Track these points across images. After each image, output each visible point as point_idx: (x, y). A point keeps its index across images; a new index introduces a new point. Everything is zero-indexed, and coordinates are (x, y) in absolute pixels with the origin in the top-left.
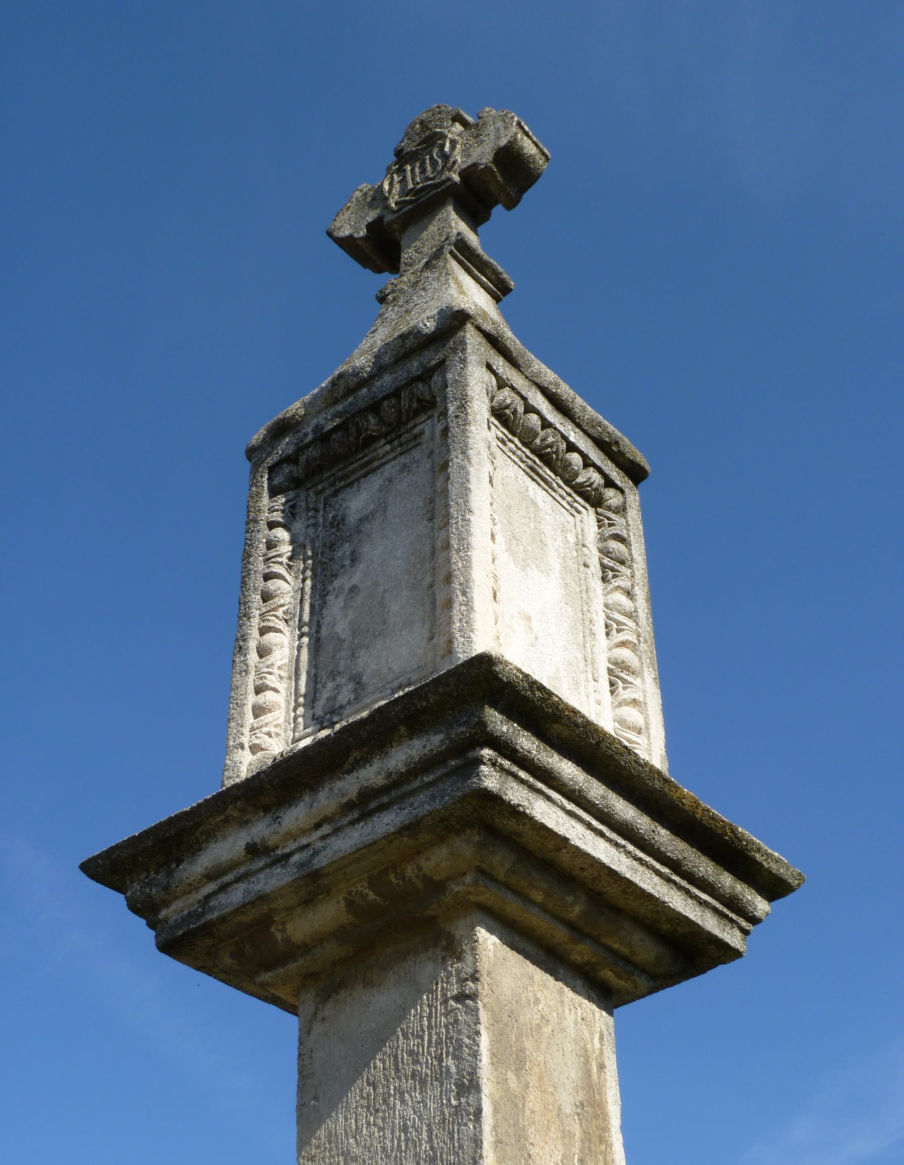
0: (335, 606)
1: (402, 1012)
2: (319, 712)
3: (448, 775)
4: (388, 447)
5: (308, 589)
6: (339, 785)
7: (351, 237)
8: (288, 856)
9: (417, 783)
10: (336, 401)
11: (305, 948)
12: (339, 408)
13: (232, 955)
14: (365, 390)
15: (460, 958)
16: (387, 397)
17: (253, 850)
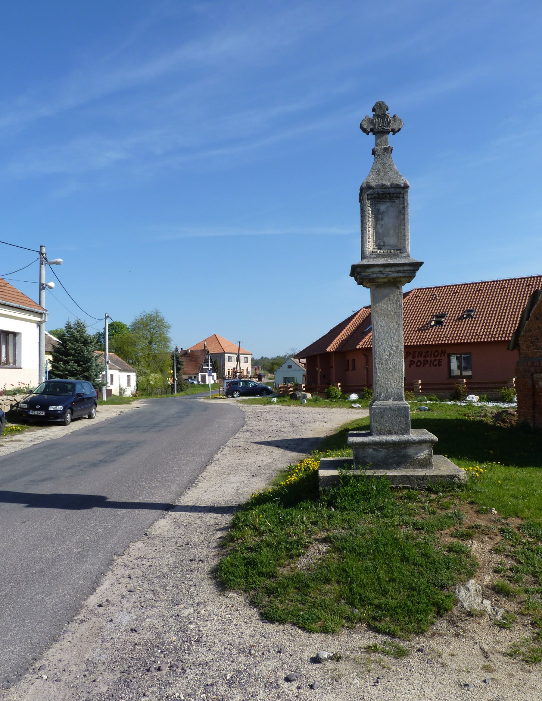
0: (379, 227)
6: (395, 268)
7: (366, 129)
11: (379, 282)
12: (383, 190)
15: (400, 289)
17: (380, 271)
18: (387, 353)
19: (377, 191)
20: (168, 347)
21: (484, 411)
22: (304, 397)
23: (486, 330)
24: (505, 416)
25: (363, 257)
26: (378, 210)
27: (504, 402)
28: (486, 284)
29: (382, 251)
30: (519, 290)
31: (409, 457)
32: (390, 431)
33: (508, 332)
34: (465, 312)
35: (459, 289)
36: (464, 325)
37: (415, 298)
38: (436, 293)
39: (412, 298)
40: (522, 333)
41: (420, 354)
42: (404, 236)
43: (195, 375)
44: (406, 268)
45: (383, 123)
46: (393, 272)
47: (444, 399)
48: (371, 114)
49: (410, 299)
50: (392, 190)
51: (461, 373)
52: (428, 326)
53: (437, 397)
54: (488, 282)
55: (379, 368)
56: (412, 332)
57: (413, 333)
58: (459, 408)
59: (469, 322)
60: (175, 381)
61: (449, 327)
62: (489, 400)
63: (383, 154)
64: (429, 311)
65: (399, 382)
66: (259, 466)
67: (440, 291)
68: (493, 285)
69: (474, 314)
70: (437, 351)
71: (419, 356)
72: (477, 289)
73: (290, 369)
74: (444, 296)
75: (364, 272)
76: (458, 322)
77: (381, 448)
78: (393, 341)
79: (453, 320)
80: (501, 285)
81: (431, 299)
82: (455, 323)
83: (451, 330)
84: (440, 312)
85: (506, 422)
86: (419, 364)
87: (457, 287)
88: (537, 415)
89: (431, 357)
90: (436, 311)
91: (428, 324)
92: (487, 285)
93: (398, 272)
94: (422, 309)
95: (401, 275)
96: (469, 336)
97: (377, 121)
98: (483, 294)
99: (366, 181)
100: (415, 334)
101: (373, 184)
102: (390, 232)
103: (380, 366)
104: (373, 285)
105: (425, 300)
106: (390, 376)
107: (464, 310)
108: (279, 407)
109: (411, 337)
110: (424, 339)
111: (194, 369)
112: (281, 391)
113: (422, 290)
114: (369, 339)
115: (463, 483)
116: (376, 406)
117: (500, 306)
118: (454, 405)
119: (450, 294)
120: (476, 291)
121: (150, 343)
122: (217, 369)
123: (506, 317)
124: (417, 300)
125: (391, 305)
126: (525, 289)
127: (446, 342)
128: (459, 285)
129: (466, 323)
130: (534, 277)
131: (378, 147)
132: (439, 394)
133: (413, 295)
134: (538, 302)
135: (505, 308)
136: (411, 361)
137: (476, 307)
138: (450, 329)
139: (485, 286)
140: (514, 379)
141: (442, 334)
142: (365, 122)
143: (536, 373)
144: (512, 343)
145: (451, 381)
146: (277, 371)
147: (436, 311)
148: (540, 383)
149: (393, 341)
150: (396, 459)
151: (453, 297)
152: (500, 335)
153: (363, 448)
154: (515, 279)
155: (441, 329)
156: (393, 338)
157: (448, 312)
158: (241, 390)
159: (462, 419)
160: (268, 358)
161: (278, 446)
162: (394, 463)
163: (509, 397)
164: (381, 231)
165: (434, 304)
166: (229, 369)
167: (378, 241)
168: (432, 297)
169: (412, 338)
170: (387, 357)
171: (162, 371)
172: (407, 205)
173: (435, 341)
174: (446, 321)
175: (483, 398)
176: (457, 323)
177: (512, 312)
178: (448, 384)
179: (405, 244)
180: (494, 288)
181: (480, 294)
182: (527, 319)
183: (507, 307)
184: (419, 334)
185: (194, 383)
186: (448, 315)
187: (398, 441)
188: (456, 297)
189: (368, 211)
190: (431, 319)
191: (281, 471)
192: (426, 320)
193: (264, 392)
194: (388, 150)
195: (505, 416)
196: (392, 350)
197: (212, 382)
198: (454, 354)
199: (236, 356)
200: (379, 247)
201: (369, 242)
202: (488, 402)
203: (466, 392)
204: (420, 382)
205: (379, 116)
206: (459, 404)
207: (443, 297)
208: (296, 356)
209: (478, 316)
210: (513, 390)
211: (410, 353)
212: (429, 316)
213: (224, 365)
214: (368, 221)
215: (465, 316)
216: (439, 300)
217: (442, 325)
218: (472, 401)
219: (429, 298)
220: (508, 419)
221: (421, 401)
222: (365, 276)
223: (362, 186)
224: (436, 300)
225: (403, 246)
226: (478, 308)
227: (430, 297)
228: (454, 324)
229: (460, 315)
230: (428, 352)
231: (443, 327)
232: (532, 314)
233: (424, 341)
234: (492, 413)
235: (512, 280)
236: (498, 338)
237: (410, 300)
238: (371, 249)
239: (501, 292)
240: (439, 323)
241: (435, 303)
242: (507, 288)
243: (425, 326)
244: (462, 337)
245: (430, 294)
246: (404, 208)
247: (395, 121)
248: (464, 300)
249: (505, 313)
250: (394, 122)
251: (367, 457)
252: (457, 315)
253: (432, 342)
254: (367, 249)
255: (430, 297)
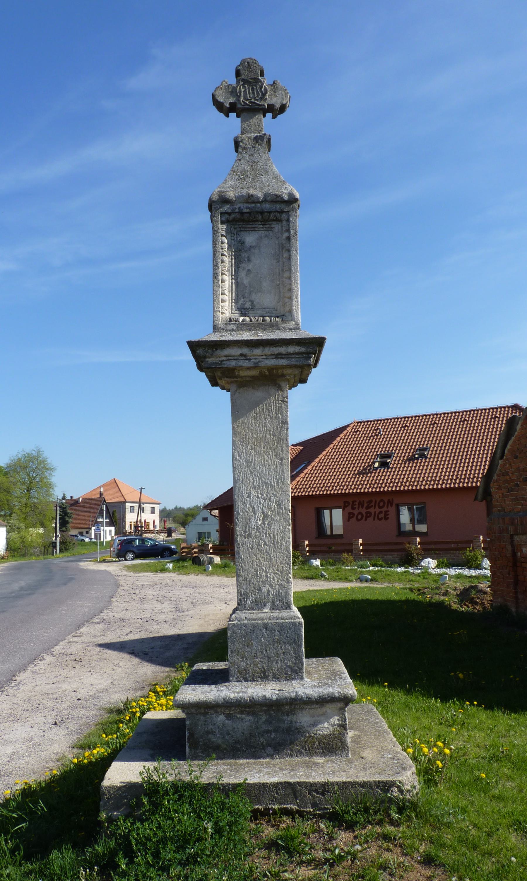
0: (242, 274)
1: (265, 399)
2: (239, 307)
3: (302, 357)
4: (262, 226)
5: (233, 263)
6: (272, 349)
7: (223, 103)
8: (251, 359)
9: (294, 356)
10: (248, 203)
11: (241, 377)
12: (249, 206)
13: (221, 373)
14: (259, 205)
15: (283, 391)
16: (267, 212)
17: (241, 355)
18: (259, 514)
19: (239, 208)
20: (51, 495)
21: (445, 586)
22: (211, 561)
23: (443, 474)
24: (475, 594)
25: (215, 329)
26: (241, 242)
27: (470, 568)
28: (442, 416)
29: (248, 319)
30: (482, 423)
31: (300, 731)
32: (264, 673)
33: (472, 476)
34: (417, 450)
35: (409, 422)
36: (415, 467)
37: (355, 434)
38: (380, 427)
39: (350, 433)
40: (495, 477)
41: (361, 504)
42: (290, 290)
43: (87, 530)
44: (292, 349)
45: (253, 93)
46: (267, 357)
47: (392, 564)
48: (232, 80)
49: (348, 434)
50: (267, 207)
51: (414, 527)
52: (370, 469)
53: (383, 560)
54: (444, 414)
55: (243, 543)
56: (351, 476)
57: (352, 477)
58: (412, 578)
59: (422, 464)
60: (58, 539)
61: (397, 469)
62: (450, 565)
63: (253, 147)
64: (371, 449)
65: (282, 573)
66: (79, 699)
67: (384, 424)
68: (451, 417)
69: (428, 454)
70: (382, 500)
71: (360, 507)
72: (431, 422)
73: (205, 522)
74: (390, 431)
75: (212, 356)
76: (409, 464)
77: (242, 712)
78: (271, 492)
79: (402, 460)
80: (460, 417)
81: (373, 434)
82: (405, 464)
83: (400, 473)
84: (389, 450)
85: (477, 603)
86: (360, 517)
87: (407, 419)
88: (520, 596)
89: (375, 508)
90: (380, 450)
91: (370, 466)
92: (443, 418)
93: (277, 356)
94: (363, 447)
95: (282, 362)
96: (422, 482)
97: (243, 90)
98: (438, 428)
99: (219, 189)
100: (355, 478)
101: (231, 195)
102: (265, 284)
103: (246, 540)
104: (232, 382)
105: (367, 435)
106: (265, 560)
107: (415, 448)
108: (174, 576)
109: (349, 482)
110: (366, 485)
111: (86, 523)
112: (183, 552)
113: (363, 424)
114: (296, 485)
115: (409, 801)
116: (235, 622)
117: (460, 443)
118: (405, 572)
119: (398, 428)
120: (430, 425)
121: (29, 490)
122: (116, 522)
123: (468, 457)
124: (356, 436)
125: (267, 422)
126: (490, 422)
127: (386, 489)
128: (408, 418)
129: (418, 464)
130: (501, 408)
131: (244, 136)
132: (385, 557)
133: (352, 430)
134: (516, 433)
135: (467, 446)
136: (350, 514)
137: (431, 444)
138: (398, 472)
139: (441, 419)
140: (481, 538)
141: (373, 480)
142: (221, 92)
143: (517, 534)
144: (481, 490)
145: (399, 540)
146: (190, 525)
147: (380, 450)
148: (524, 550)
149: (271, 492)
150: (273, 735)
151: (401, 432)
152: (462, 480)
153: (205, 714)
154: (478, 410)
155: (387, 472)
156: (271, 485)
157: (395, 450)
158: (136, 551)
159: (414, 600)
160: (183, 508)
161: (132, 653)
162: (269, 745)
163: (475, 561)
164: (246, 282)
165: (377, 440)
166: (131, 522)
167: (241, 301)
168: (375, 432)
169: (351, 483)
170: (260, 522)
171: (43, 525)
172: (296, 233)
173: (380, 488)
174: (393, 462)
175: (443, 563)
176: (407, 465)
177: (475, 451)
178: (397, 544)
179: (291, 305)
180: (452, 421)
181: (434, 429)
182: (502, 457)
183: (469, 445)
184: (360, 479)
185: (84, 540)
186: (396, 455)
187: (277, 699)
188: (405, 431)
189: (222, 243)
190: (374, 459)
191: (111, 711)
192: (368, 461)
193: (167, 553)
194: (262, 140)
195: (475, 594)
196: (269, 508)
197: (109, 538)
198: (403, 505)
199: (138, 505)
200: (243, 311)
201: (223, 301)
202: (450, 568)
203: (420, 555)
204: (360, 541)
205: (245, 82)
206: (412, 571)
207: (389, 432)
208: (206, 507)
209: (433, 456)
210: (481, 552)
211: (349, 503)
212: (372, 456)
213: (124, 517)
214: (222, 262)
215: (417, 456)
216: (384, 435)
217: (388, 467)
218: (428, 566)
219: (372, 433)
220: (478, 598)
221: (362, 567)
222: (214, 364)
223: (210, 199)
224: (381, 436)
225: (287, 309)
226: (432, 445)
227: (373, 432)
228: (403, 465)
229: (411, 454)
230: (371, 501)
231: (390, 470)
232: (509, 450)
233: (366, 488)
234: (456, 589)
235: (474, 411)
236: (450, 484)
237: (349, 436)
238: (228, 315)
239: (461, 426)
240: (384, 465)
241: (379, 439)
242: (468, 421)
243: (367, 468)
244: (414, 482)
245: (373, 429)
246: (289, 238)
247: (275, 92)
248: (416, 436)
249: (467, 452)
250: (272, 93)
251: (212, 732)
252: (407, 455)
253: (376, 488)
254: (220, 315)
255: (373, 432)
